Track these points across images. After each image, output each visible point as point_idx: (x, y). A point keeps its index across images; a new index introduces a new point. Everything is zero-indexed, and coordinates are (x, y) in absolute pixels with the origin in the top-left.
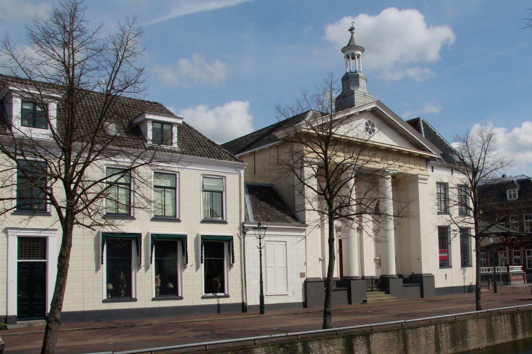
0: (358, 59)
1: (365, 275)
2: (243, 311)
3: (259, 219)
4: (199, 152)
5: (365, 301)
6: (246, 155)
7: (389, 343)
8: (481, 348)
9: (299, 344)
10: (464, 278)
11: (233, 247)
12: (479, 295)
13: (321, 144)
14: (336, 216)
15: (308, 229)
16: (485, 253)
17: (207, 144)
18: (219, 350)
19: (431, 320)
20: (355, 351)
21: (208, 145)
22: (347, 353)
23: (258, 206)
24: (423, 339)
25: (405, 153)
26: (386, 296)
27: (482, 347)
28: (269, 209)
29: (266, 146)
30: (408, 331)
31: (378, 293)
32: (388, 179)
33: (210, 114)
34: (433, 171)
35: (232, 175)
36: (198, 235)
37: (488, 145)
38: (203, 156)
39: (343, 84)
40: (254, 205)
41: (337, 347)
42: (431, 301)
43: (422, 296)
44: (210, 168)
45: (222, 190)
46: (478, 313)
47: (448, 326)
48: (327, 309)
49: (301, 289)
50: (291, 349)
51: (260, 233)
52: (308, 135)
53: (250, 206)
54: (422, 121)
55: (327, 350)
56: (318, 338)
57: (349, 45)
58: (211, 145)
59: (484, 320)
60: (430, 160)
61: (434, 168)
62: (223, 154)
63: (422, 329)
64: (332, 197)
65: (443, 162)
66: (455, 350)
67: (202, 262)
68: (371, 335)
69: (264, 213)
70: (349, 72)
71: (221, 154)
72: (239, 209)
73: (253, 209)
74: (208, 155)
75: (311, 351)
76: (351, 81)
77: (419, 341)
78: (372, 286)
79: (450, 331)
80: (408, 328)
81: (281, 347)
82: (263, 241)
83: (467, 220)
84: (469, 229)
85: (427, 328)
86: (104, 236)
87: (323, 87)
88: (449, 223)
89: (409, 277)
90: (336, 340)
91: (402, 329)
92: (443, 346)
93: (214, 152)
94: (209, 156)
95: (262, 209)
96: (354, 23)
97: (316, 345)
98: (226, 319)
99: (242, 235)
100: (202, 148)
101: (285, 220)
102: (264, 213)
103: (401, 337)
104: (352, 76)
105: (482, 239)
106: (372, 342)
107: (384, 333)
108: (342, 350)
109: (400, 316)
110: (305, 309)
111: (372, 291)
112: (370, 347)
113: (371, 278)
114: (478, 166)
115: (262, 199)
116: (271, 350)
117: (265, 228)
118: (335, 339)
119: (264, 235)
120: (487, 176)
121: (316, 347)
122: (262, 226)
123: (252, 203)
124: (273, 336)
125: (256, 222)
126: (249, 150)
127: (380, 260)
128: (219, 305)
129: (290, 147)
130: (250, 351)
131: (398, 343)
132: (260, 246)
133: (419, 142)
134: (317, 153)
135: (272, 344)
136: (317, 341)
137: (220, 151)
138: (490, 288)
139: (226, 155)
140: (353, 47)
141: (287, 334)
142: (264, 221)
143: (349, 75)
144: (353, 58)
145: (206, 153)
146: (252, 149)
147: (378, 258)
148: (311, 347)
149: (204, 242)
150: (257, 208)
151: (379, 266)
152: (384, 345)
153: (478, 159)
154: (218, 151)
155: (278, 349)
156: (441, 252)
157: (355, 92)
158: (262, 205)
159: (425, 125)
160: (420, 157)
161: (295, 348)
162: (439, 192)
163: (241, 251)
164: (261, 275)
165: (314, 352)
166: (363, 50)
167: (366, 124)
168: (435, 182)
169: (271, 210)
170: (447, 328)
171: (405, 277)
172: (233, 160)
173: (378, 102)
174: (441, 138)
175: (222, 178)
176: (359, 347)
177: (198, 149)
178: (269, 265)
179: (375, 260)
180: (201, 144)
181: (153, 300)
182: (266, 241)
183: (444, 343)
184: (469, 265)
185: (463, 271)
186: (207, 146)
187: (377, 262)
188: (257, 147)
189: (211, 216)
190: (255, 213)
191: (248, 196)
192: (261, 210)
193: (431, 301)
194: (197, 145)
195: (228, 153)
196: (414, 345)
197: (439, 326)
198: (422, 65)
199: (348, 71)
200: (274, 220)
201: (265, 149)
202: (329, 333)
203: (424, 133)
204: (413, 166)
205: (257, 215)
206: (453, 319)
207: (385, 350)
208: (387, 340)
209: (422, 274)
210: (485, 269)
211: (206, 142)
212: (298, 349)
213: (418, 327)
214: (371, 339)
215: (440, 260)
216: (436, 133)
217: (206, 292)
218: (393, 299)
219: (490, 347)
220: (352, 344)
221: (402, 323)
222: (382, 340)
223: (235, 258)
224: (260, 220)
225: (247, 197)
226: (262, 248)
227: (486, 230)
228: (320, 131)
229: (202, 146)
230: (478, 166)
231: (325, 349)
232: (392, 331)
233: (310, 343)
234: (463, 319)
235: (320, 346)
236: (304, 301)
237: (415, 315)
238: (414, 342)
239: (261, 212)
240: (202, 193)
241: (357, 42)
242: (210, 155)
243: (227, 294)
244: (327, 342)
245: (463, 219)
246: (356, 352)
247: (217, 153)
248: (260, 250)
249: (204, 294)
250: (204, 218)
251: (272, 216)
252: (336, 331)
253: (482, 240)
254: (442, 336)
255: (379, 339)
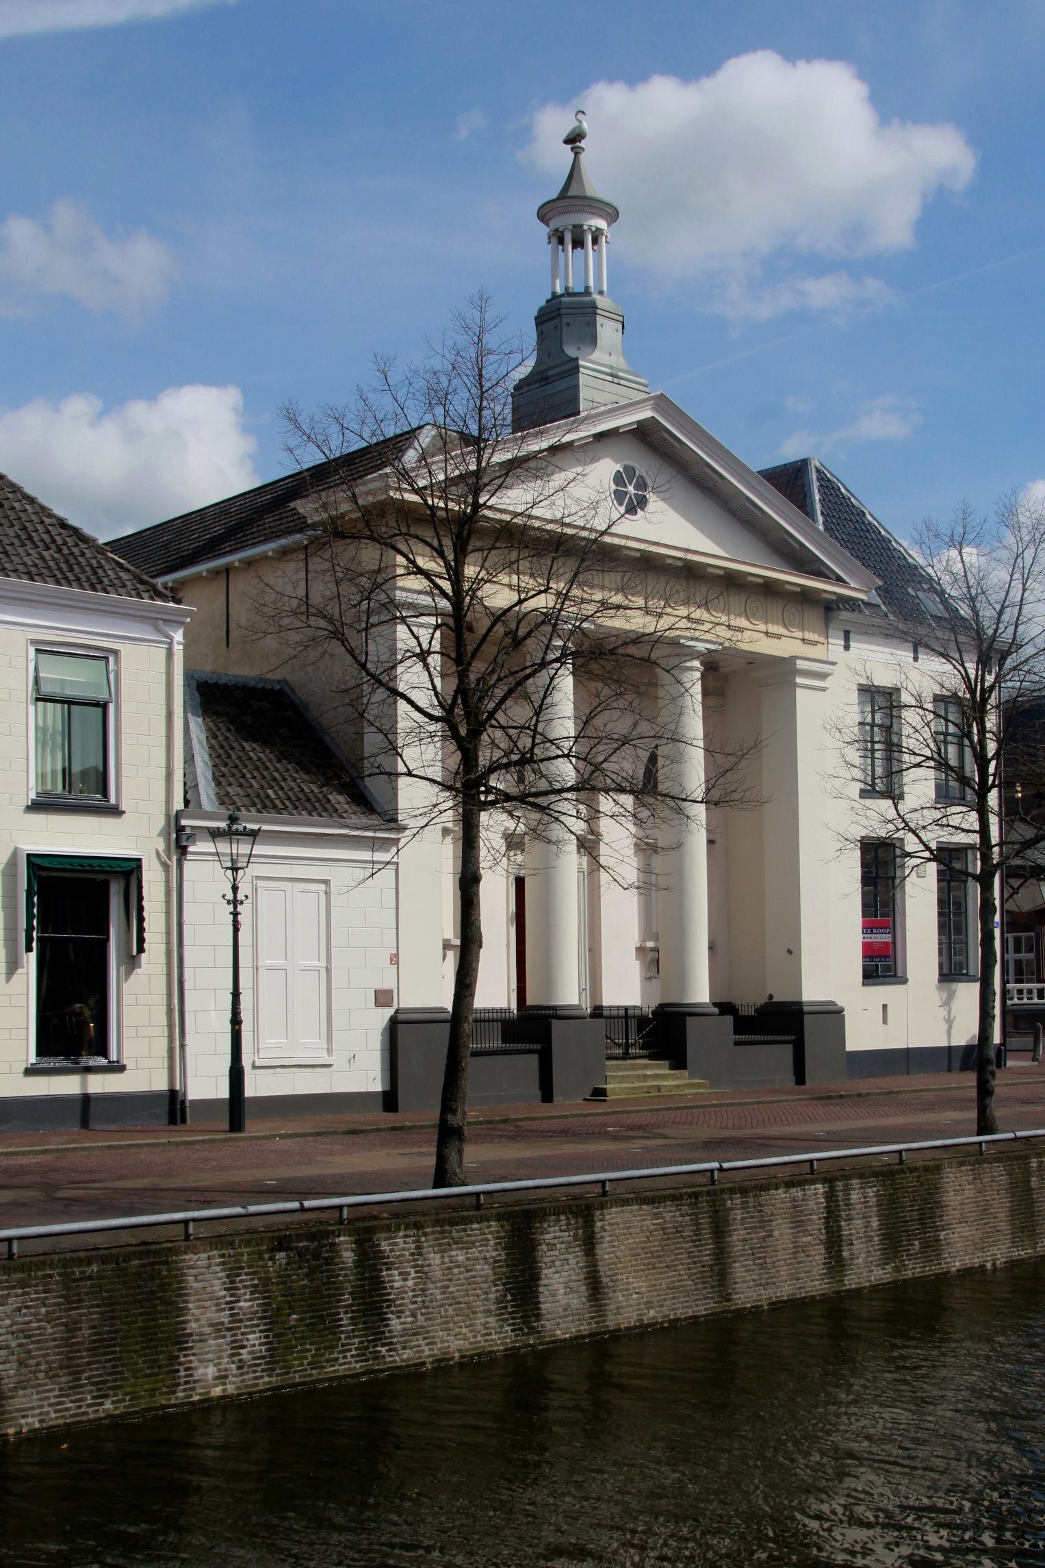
0: (596, 247)
1: (606, 1003)
2: (172, 1121)
3: (234, 803)
4: (25, 564)
5: (599, 1093)
6: (198, 578)
7: (664, 1240)
8: (989, 1266)
9: (342, 1239)
10: (950, 1022)
11: (140, 898)
12: (988, 1082)
13: (441, 545)
14: (491, 798)
15: (404, 837)
16: (1033, 934)
17: (53, 533)
18: (56, 1257)
19: (812, 1165)
20: (541, 1268)
21: (58, 538)
22: (512, 1271)
23: (234, 757)
24: (782, 1231)
25: (710, 573)
26: (674, 1078)
27: (994, 1264)
28: (272, 769)
29: (269, 548)
30: (732, 1200)
31: (646, 1067)
32: (691, 669)
33: (109, 432)
34: (847, 647)
35: (142, 649)
36: (16, 852)
37: (1034, 559)
38: (36, 578)
39: (541, 335)
40: (221, 751)
41: (480, 1252)
42: (829, 1098)
43: (800, 1078)
44: (24, 615)
45: (103, 696)
46: (980, 1143)
47: (871, 1187)
48: (450, 1117)
49: (379, 1047)
50: (316, 1256)
51: (234, 851)
52: (404, 512)
53: (206, 757)
54: (818, 471)
55: (443, 1263)
56: (412, 1219)
57: (563, 195)
58: (68, 539)
59: (1000, 1168)
60: (839, 608)
61: (852, 636)
62: (110, 572)
63: (781, 1193)
64: (475, 734)
65: (886, 616)
66: (897, 1269)
67: (29, 949)
68: (598, 1213)
69: (252, 781)
70: (563, 291)
71: (105, 571)
72: (164, 765)
73: (215, 766)
74: (57, 572)
75: (386, 1264)
76: (568, 325)
77: (771, 1236)
78: (627, 1039)
79: (879, 1205)
80: (732, 1191)
81: (280, 1248)
82: (248, 879)
83: (955, 821)
84: (969, 852)
85: (797, 1192)
86: (34, 864)
87: (450, 343)
88: (891, 827)
89: (757, 1011)
90: (475, 1226)
91: (708, 1193)
92: (853, 1257)
93: (79, 563)
94: (59, 576)
95: (246, 766)
96: (583, 112)
97: (405, 1243)
98: (109, 1147)
99: (175, 858)
100: (37, 547)
101: (328, 806)
102: (252, 781)
103: (705, 1221)
104: (570, 306)
105: (1021, 886)
106: (602, 1237)
107: (644, 1207)
108: (496, 1262)
109: (713, 1146)
110: (391, 1116)
111: (626, 1056)
112: (595, 1255)
113: (622, 1013)
114: (996, 631)
115: (248, 732)
116: (245, 1258)
117: (254, 834)
118: (472, 1222)
119: (250, 856)
120: (1026, 668)
121: (403, 1249)
122: (241, 828)
123: (212, 747)
124: (253, 1209)
125: (222, 810)
126: (209, 559)
127: (656, 950)
128: (86, 1099)
129: (327, 555)
130: (166, 1263)
131: (693, 1241)
132: (235, 897)
133: (801, 545)
134: (427, 575)
135: (248, 1237)
136: (405, 1230)
137: (99, 562)
138: (1040, 1058)
139: (122, 574)
140: (579, 202)
141: (302, 1205)
142: (252, 809)
143: (560, 302)
144: (578, 243)
145: (49, 568)
146: (220, 556)
147: (650, 944)
148: (387, 1248)
149: (41, 880)
150: (231, 764)
151: (654, 973)
152: (643, 1248)
153: (998, 607)
154: (94, 562)
155: (266, 1256)
156: (868, 928)
157: (581, 363)
158: (246, 753)
159: (827, 487)
160: (805, 598)
161: (327, 1251)
162: (869, 719)
163: (168, 913)
164: (236, 995)
165: (397, 1269)
166: (612, 215)
167: (618, 479)
168: (856, 687)
169: (277, 770)
170: (871, 1192)
171: (743, 1012)
172: (145, 595)
173: (661, 402)
174: (883, 533)
175: (103, 656)
176: (557, 1253)
177: (20, 550)
178: (269, 962)
179: (641, 950)
180: (33, 534)
181: (30, 1072)
182: (258, 878)
183: (858, 1246)
184: (967, 974)
185: (945, 995)
186: (54, 541)
187: (648, 959)
188: (237, 549)
189: (64, 787)
190: (221, 779)
191: (200, 720)
192: (244, 771)
193: (829, 1098)
194: (18, 536)
195: (127, 570)
196: (752, 1249)
197: (840, 1184)
198: (857, 269)
199: (559, 290)
200: (316, 809)
201: (263, 558)
202: (452, 1201)
203: (822, 513)
204: (781, 630)
205: (229, 789)
206: (893, 1162)
207: (649, 1264)
208: (656, 1230)
209: (800, 1004)
210: (1030, 991)
211: (50, 528)
212: (341, 1257)
213: (765, 1188)
214: (599, 1224)
215: (864, 957)
216: (864, 514)
217: (40, 1053)
218: (699, 1086)
219: (1021, 1261)
220: (533, 1240)
221: (712, 1171)
222: (638, 1230)
223: (145, 935)
224: (239, 804)
225: (197, 724)
226: (242, 903)
227: (1017, 855)
228: (440, 498)
229: (33, 542)
230: (996, 631)
231: (435, 1259)
232: (674, 1198)
233: (383, 1235)
234: (927, 1163)
235: (417, 1248)
236: (388, 1088)
237: (764, 1145)
238: (752, 1239)
239: (244, 776)
240: (32, 708)
241: (595, 184)
242: (62, 572)
243: (118, 1062)
244: (443, 1232)
245: (940, 815)
246: (545, 1271)
247: (87, 569)
248: (235, 907)
249: (33, 1058)
250: (38, 795)
251: (280, 793)
252: (477, 1194)
253: (1021, 890)
254: (850, 1219)
255: (628, 1228)
